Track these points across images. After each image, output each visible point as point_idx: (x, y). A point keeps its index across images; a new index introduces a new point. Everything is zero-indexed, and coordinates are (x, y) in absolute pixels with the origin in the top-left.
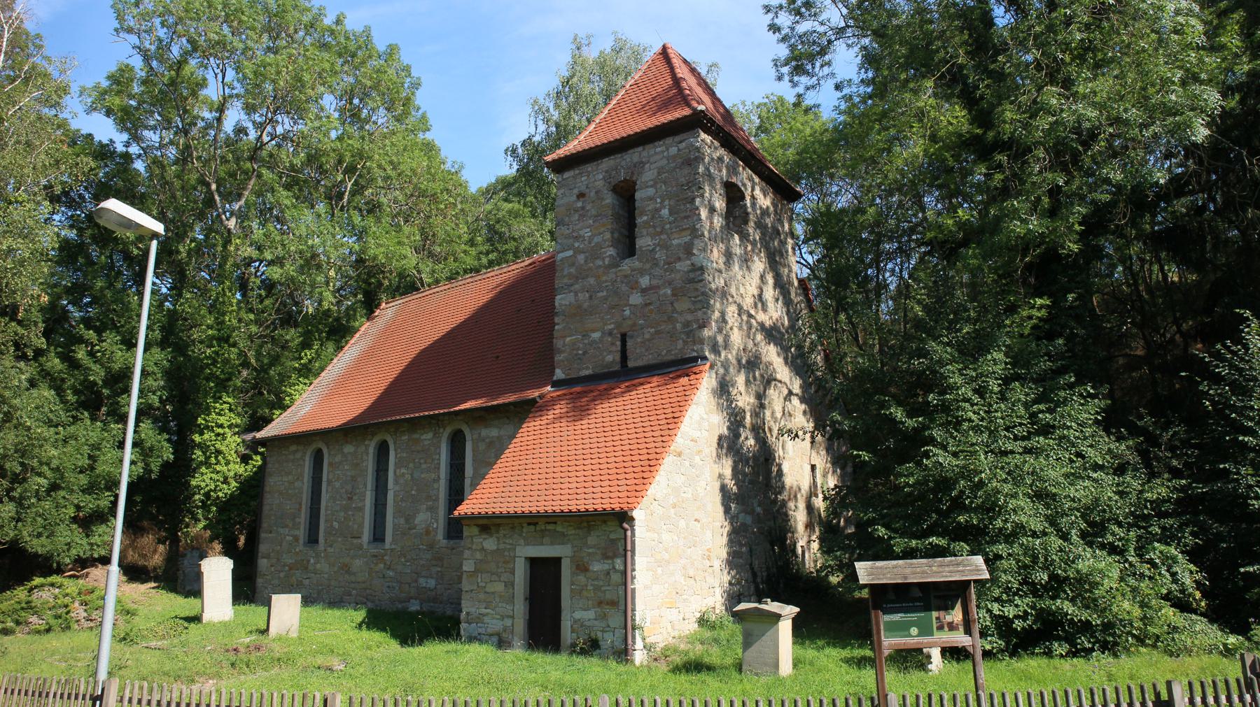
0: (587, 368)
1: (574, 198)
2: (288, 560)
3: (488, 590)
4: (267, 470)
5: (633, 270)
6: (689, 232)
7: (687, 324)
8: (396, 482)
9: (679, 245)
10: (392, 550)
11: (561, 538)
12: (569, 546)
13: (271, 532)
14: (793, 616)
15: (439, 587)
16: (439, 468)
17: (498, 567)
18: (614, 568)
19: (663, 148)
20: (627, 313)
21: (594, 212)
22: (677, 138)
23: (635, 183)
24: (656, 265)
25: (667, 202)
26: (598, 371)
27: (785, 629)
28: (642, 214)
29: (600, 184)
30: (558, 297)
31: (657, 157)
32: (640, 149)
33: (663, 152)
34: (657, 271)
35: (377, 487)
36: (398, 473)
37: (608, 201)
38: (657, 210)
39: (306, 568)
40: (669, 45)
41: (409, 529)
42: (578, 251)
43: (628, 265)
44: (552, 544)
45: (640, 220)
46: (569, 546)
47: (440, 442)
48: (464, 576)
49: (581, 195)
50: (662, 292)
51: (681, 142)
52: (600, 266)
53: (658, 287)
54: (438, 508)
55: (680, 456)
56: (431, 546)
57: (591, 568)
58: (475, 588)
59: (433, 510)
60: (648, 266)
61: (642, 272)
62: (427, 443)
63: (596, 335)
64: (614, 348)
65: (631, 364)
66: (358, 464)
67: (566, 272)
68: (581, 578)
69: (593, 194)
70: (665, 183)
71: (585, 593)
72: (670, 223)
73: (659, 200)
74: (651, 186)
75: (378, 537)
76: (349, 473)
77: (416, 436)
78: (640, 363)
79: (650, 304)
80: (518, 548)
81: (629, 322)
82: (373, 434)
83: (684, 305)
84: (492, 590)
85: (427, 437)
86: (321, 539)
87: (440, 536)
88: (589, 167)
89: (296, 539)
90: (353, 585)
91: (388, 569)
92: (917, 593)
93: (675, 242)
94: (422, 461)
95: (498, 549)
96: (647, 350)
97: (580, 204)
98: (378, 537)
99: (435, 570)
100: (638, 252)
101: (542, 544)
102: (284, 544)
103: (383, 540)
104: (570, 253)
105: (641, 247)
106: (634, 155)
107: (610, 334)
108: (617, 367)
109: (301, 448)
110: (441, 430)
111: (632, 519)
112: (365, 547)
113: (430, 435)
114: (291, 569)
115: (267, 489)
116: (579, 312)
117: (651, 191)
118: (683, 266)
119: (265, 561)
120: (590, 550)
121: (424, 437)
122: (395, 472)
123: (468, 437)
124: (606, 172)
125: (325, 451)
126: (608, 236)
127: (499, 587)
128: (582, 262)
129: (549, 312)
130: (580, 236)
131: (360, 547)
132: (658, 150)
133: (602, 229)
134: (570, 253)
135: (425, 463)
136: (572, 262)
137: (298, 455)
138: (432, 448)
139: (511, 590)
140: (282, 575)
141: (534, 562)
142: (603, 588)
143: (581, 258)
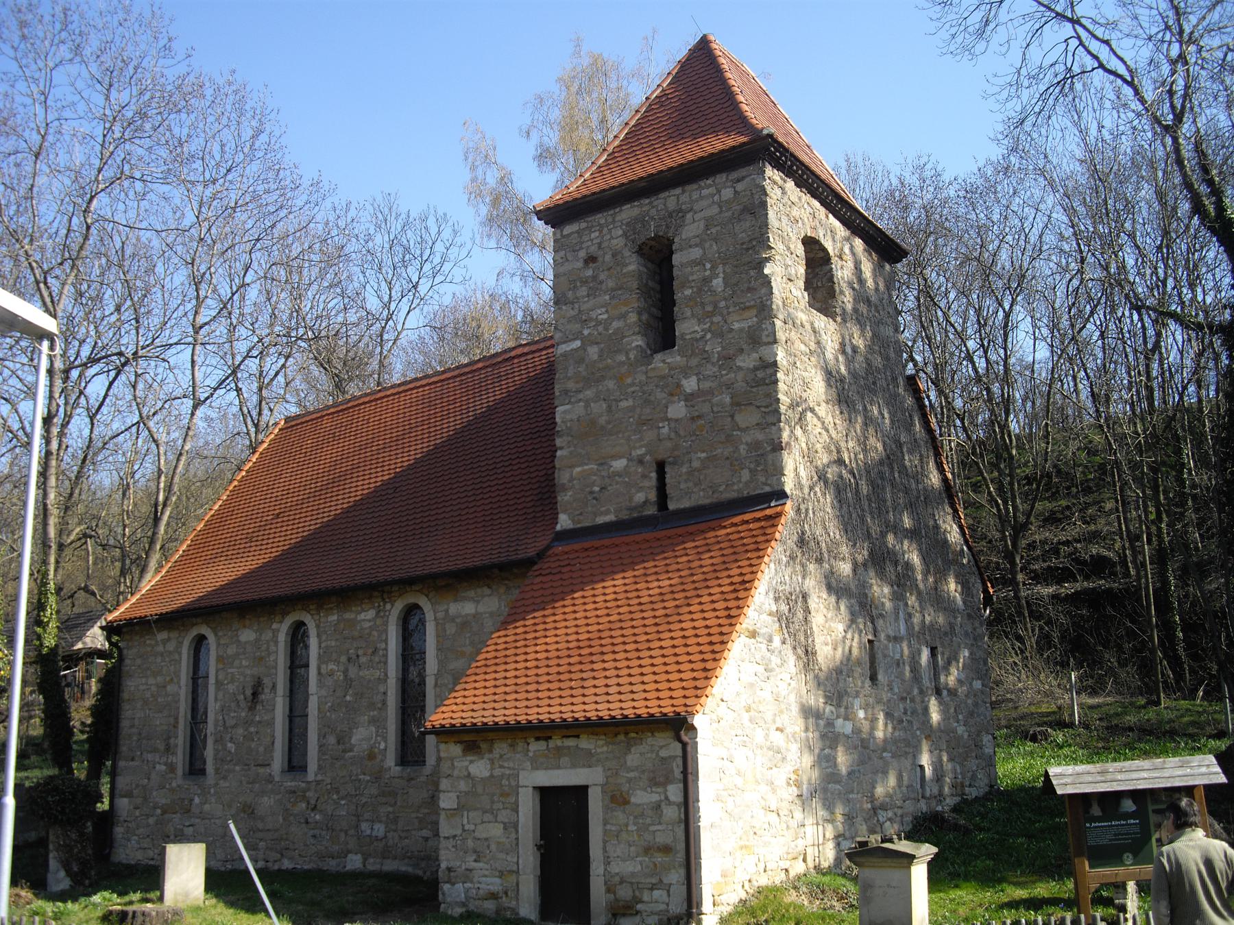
0: (607, 512)
1: (580, 264)
2: (161, 798)
3: (477, 834)
4: (125, 669)
5: (671, 369)
6: (754, 312)
7: (755, 445)
8: (320, 684)
9: (741, 330)
10: (318, 782)
11: (587, 759)
12: (600, 769)
13: (133, 759)
14: (929, 858)
15: (390, 835)
16: (386, 663)
17: (493, 802)
18: (667, 798)
19: (712, 190)
20: (665, 430)
21: (611, 284)
22: (735, 175)
23: (671, 242)
24: (708, 359)
25: (720, 269)
26: (624, 515)
27: (919, 874)
28: (683, 286)
29: (618, 243)
30: (560, 409)
31: (704, 203)
32: (678, 191)
33: (713, 195)
34: (710, 370)
35: (291, 691)
36: (323, 671)
37: (632, 267)
38: (706, 281)
39: (188, 811)
40: (712, 38)
41: (344, 751)
42: (587, 342)
43: (663, 362)
44: (574, 766)
45: (683, 294)
46: (600, 769)
47: (386, 624)
48: (442, 816)
49: (590, 260)
50: (715, 400)
51: (738, 181)
52: (623, 363)
53: (711, 392)
54: (386, 719)
55: (754, 637)
56: (378, 776)
57: (633, 800)
58: (459, 832)
59: (378, 722)
60: (694, 362)
61: (686, 372)
62: (367, 625)
63: (619, 464)
64: (647, 483)
65: (672, 506)
66: (261, 658)
67: (571, 373)
68: (620, 816)
69: (608, 258)
70: (716, 240)
71: (624, 836)
72: (725, 299)
73: (708, 266)
74: (696, 245)
75: (295, 765)
76: (248, 672)
77: (348, 616)
78: (686, 504)
79: (699, 417)
80: (522, 774)
81: (669, 444)
82: (284, 614)
83: (747, 418)
84: (484, 835)
85: (366, 616)
86: (210, 768)
87: (390, 761)
88: (600, 218)
89: (172, 768)
90: (260, 835)
91: (313, 809)
92: (1129, 805)
93: (736, 326)
94: (360, 652)
95: (492, 776)
96: (696, 485)
97: (589, 273)
98: (295, 765)
99: (384, 810)
100: (678, 342)
101: (559, 767)
102: (153, 776)
103: (303, 769)
104: (578, 343)
105: (683, 335)
106: (671, 199)
107: (641, 462)
108: (652, 511)
109: (174, 634)
110: (388, 606)
111: (693, 728)
112: (277, 779)
113: (371, 614)
114: (164, 812)
115: (125, 696)
116: (591, 431)
117: (696, 253)
118: (747, 361)
119: (125, 800)
120: (632, 775)
121: (362, 616)
122: (319, 669)
123: (429, 616)
124: (628, 224)
125: (211, 638)
126: (633, 318)
127: (496, 831)
128: (595, 357)
129: (549, 427)
130: (591, 319)
131: (270, 779)
132: (705, 192)
133: (624, 309)
134: (578, 343)
135: (365, 654)
136: (578, 357)
137: (171, 646)
138: (375, 633)
139: (513, 836)
140: (151, 821)
141: (547, 794)
142: (652, 828)
143: (593, 352)
